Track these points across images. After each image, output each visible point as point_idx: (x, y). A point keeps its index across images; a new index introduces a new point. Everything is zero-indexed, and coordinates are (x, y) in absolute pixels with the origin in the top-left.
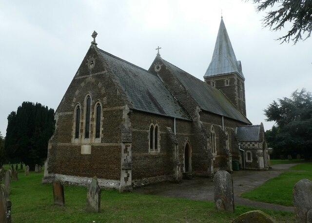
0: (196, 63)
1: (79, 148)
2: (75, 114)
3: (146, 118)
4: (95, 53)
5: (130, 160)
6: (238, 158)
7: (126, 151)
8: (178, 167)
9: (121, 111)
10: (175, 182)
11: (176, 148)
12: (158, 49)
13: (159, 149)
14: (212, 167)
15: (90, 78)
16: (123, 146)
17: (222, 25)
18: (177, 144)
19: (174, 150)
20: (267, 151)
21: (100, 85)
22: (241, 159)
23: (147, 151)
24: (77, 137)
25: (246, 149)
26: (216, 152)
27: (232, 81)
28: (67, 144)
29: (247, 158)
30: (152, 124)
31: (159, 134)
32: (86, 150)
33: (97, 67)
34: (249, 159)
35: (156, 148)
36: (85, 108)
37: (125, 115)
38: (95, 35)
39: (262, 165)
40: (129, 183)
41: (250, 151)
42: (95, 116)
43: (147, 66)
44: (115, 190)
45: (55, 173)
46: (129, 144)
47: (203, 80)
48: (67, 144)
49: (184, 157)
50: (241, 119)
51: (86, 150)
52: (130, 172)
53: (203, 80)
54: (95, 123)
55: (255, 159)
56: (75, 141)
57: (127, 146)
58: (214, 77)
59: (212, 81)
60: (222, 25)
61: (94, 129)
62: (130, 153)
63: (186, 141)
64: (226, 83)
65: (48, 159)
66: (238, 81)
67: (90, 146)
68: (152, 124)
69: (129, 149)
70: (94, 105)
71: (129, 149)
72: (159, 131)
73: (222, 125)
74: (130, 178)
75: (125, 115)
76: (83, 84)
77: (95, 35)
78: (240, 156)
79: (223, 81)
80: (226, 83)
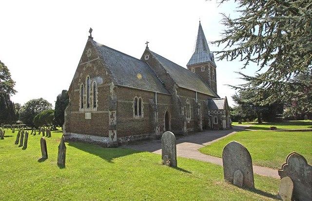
0: (179, 53)
1: (84, 115)
2: (81, 91)
3: (131, 92)
4: (91, 44)
5: (115, 123)
6: (208, 121)
7: (112, 117)
8: (157, 127)
9: (109, 87)
10: (199, 131)
11: (156, 114)
12: (147, 43)
13: (142, 115)
14: (185, 128)
15: (89, 64)
16: (110, 113)
17: (200, 27)
18: (156, 112)
19: (154, 116)
20: (229, 116)
21: (95, 68)
22: (210, 122)
23: (132, 116)
24: (82, 107)
25: (214, 115)
26: (191, 117)
27: (207, 67)
28: (77, 112)
29: (214, 121)
30: (136, 97)
31: (142, 104)
32: (88, 116)
33: (95, 58)
34: (216, 122)
35: (140, 114)
36: (86, 86)
37: (112, 91)
38: (91, 31)
39: (224, 126)
40: (115, 139)
41: (216, 117)
42: (92, 92)
43: (139, 56)
44: (206, 128)
45: (70, 132)
46: (114, 111)
47: (186, 68)
48: (77, 112)
49: (164, 120)
50: (216, 96)
51: (88, 116)
52: (115, 132)
53: (186, 68)
54: (93, 97)
55: (220, 122)
56: (81, 110)
57: (112, 113)
58: (194, 65)
59: (192, 68)
60: (200, 27)
61: (93, 101)
62: (115, 118)
63: (167, 109)
64: (202, 70)
65: (65, 123)
66: (211, 67)
67: (90, 113)
68: (136, 97)
69: (114, 115)
70: (91, 84)
71: (114, 115)
72: (142, 102)
73: (196, 98)
74: (115, 136)
75: (112, 91)
76: (84, 69)
77: (91, 31)
78: (209, 120)
79: (200, 68)
80: (202, 70)
